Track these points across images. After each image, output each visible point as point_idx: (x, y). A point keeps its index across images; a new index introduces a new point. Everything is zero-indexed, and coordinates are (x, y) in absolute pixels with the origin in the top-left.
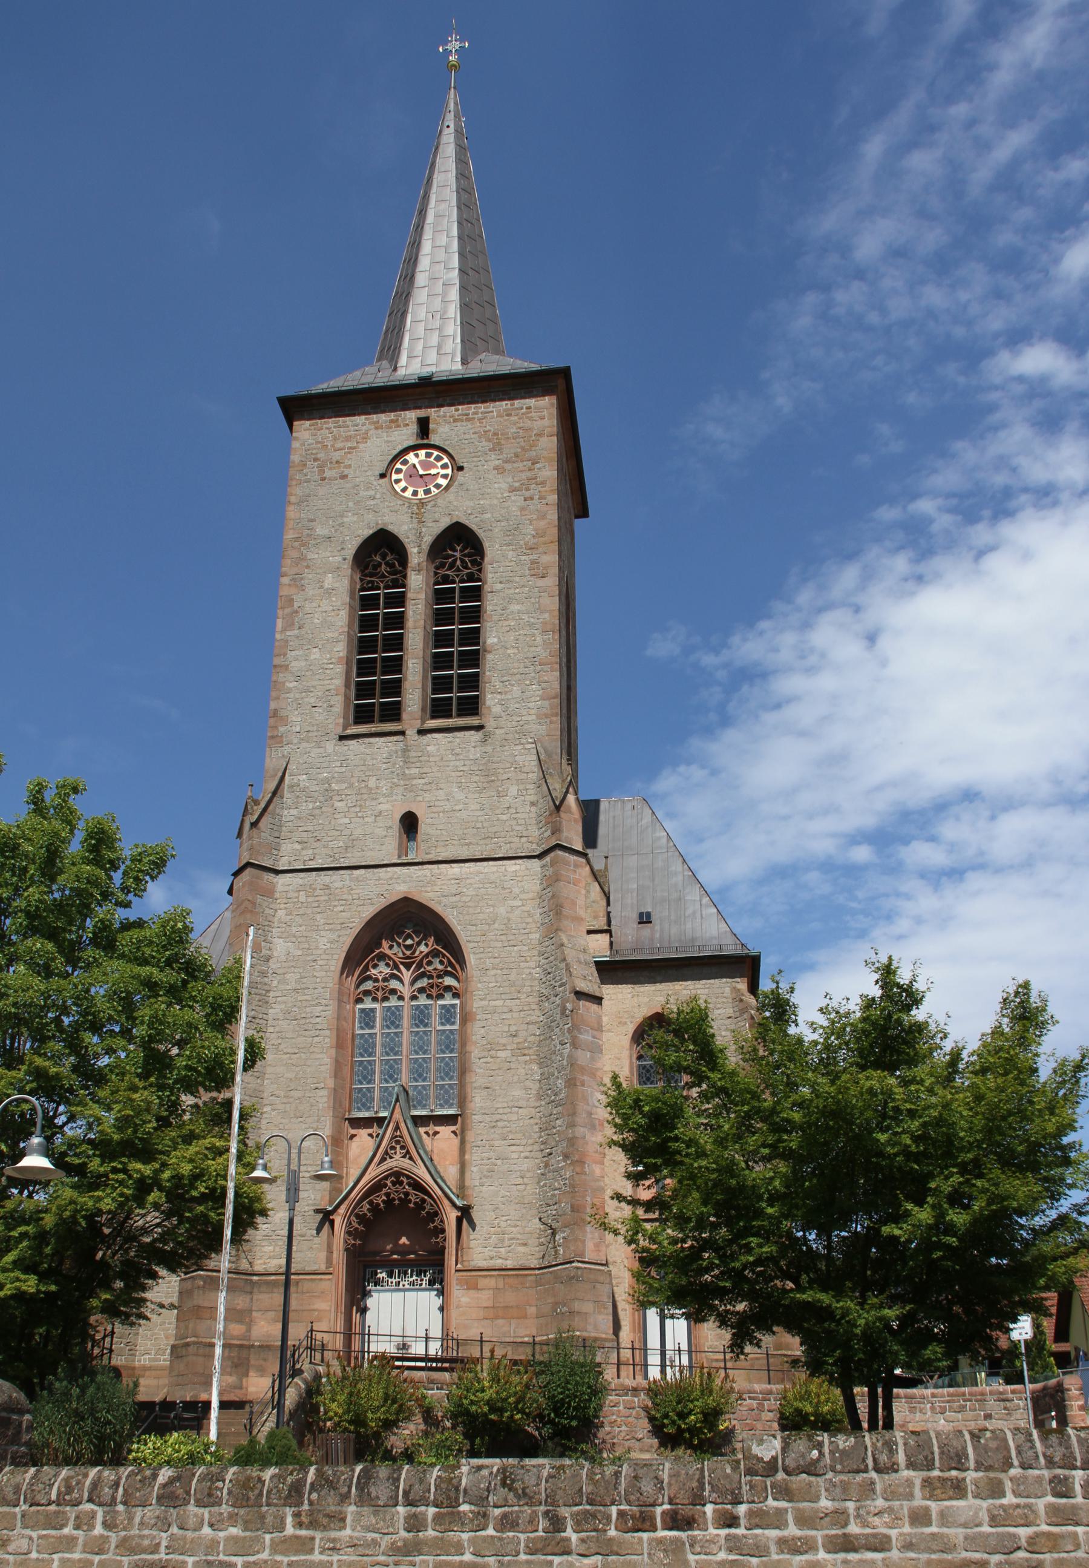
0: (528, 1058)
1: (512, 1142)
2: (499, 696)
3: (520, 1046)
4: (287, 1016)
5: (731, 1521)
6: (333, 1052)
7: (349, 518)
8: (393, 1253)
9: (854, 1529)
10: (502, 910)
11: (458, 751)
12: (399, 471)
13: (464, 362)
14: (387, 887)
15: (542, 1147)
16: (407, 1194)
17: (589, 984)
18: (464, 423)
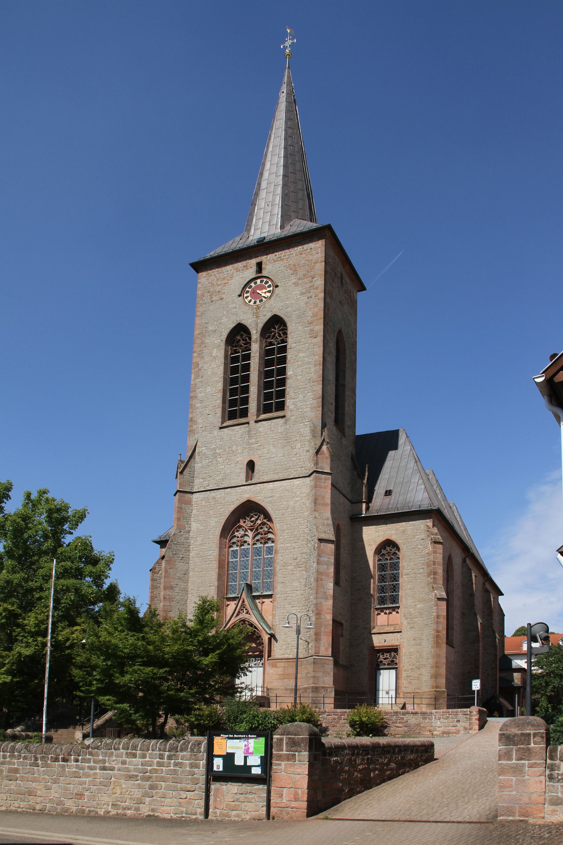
2: (293, 400)
5: (77, 761)
7: (224, 320)
9: (107, 764)
10: (291, 503)
11: (273, 429)
12: (248, 292)
13: (282, 227)
17: (327, 535)
18: (279, 262)
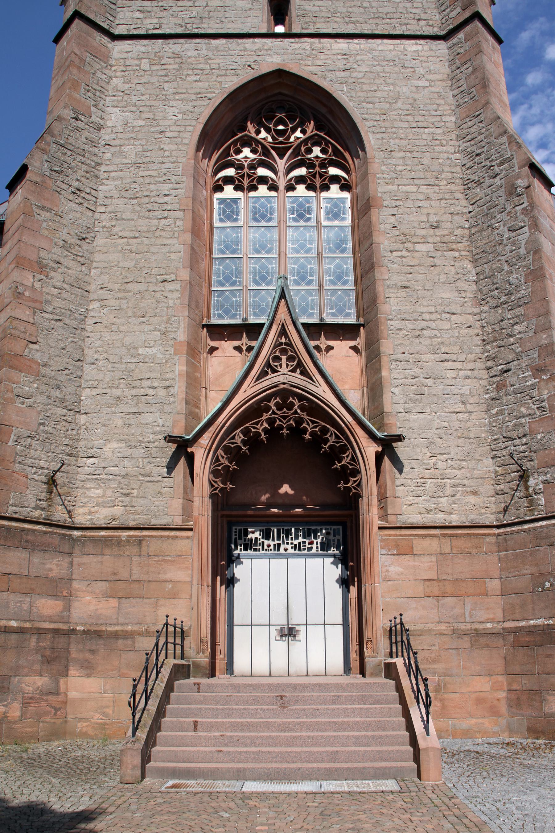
0: (457, 254)
1: (446, 357)
3: (445, 239)
4: (124, 194)
6: (188, 237)
8: (270, 505)
14: (256, 58)
15: (489, 364)
16: (299, 421)
